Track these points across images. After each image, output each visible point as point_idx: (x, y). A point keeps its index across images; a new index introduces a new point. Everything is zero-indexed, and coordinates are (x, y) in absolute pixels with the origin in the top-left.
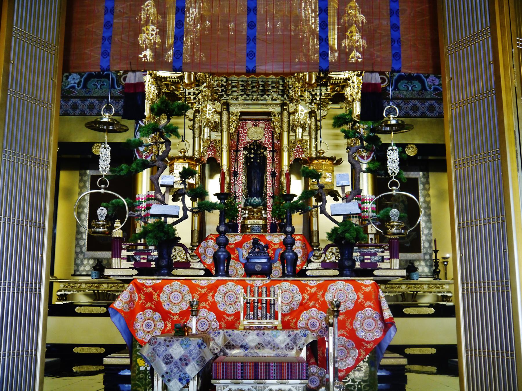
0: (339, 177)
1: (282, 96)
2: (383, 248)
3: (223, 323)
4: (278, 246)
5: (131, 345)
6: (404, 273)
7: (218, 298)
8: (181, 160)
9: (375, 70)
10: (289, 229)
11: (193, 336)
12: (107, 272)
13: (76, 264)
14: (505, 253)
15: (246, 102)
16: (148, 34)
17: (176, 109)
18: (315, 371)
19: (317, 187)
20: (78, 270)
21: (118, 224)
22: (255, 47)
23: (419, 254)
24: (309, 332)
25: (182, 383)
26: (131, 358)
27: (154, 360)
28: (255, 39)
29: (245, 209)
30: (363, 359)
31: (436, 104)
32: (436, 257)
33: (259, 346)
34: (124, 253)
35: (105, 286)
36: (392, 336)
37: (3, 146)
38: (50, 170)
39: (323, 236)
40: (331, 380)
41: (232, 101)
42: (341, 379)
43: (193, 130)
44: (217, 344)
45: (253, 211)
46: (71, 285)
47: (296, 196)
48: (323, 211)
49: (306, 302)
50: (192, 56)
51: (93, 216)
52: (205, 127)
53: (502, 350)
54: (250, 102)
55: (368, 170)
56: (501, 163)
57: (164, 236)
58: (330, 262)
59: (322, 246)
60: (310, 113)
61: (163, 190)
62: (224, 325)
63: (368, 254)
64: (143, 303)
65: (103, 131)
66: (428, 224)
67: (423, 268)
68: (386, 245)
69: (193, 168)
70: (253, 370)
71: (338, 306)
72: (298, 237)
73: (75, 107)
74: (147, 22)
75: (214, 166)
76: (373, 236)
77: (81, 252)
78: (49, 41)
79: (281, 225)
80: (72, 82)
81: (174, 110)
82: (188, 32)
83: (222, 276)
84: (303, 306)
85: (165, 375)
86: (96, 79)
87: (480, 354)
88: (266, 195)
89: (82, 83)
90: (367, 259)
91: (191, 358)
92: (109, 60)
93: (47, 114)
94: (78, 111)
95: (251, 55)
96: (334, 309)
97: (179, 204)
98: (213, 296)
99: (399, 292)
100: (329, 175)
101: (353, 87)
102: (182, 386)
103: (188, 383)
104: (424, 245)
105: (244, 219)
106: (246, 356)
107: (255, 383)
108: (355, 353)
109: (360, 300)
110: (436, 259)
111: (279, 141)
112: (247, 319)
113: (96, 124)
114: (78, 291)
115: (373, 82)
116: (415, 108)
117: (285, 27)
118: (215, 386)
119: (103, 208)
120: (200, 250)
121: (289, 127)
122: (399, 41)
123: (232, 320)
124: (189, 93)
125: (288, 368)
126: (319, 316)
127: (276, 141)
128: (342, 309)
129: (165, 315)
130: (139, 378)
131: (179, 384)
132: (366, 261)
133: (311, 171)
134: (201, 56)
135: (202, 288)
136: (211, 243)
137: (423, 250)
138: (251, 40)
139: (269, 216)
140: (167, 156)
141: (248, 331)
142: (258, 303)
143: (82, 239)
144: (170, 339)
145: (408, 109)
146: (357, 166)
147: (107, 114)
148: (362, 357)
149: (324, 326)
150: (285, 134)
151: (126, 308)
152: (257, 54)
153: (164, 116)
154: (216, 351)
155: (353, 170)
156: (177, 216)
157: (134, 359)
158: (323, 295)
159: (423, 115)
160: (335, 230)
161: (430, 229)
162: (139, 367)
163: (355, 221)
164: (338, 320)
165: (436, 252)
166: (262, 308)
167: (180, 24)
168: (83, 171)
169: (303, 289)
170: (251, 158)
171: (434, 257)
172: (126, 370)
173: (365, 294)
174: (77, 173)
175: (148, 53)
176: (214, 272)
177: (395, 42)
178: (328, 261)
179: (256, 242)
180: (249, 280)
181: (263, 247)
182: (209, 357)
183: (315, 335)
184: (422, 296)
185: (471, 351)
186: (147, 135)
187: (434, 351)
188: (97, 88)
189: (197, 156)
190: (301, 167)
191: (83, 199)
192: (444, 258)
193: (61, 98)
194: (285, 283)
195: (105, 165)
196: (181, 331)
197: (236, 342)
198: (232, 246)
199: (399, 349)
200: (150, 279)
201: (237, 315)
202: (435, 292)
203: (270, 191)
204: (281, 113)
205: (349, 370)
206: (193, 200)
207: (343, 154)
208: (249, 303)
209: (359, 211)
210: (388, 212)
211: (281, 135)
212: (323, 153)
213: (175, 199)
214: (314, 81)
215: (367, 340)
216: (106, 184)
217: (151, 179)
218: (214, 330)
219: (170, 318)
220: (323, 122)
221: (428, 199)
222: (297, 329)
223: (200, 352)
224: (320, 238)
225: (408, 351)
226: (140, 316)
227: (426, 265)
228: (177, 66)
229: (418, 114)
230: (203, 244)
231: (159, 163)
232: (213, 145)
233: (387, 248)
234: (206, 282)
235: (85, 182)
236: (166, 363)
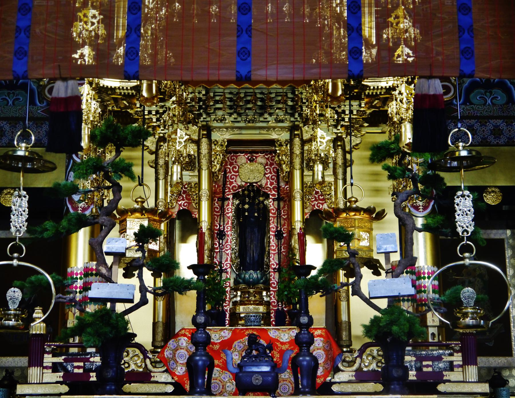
0: (381, 239)
1: (292, 115)
2: (452, 348)
4: (287, 346)
8: (138, 215)
9: (434, 75)
10: (304, 320)
15: (237, 125)
16: (86, 23)
17: (129, 137)
19: (346, 255)
21: (38, 314)
22: (250, 42)
23: (509, 358)
28: (249, 30)
29: (236, 290)
34: (48, 359)
39: (357, 330)
41: (215, 124)
47: (314, 268)
48: (357, 292)
50: (154, 56)
52: (174, 163)
54: (242, 124)
55: (426, 228)
59: (356, 345)
63: (427, 358)
65: (18, 170)
69: (155, 225)
72: (319, 332)
75: (189, 223)
79: (292, 313)
82: (147, 19)
86: (6, 92)
88: (268, 266)
90: (427, 366)
95: (244, 54)
97: (135, 281)
100: (364, 235)
101: (401, 101)
105: (235, 304)
111: (287, 183)
113: (6, 160)
115: (432, 93)
119: (16, 289)
120: (167, 353)
121: (302, 162)
122: (471, 29)
124: (150, 112)
127: (282, 184)
132: (425, 369)
133: (337, 230)
134: (167, 55)
136: (184, 341)
138: (244, 30)
139: (273, 300)
140: (116, 207)
146: (408, 222)
147: (24, 145)
150: (297, 174)
153: (111, 147)
156: (131, 301)
160: (375, 321)
163: (406, 306)
170: (245, 210)
176: (187, 387)
177: (465, 31)
178: (365, 369)
179: (253, 341)
181: (264, 348)
186: (85, 176)
198: (217, 347)
203: (274, 261)
204: (290, 142)
206: (156, 275)
207: (386, 202)
209: (412, 291)
211: (290, 174)
212: (356, 201)
213: (127, 275)
214: (340, 93)
217: (91, 244)
220: (355, 153)
228: (131, 70)
230: (172, 343)
233: (457, 348)
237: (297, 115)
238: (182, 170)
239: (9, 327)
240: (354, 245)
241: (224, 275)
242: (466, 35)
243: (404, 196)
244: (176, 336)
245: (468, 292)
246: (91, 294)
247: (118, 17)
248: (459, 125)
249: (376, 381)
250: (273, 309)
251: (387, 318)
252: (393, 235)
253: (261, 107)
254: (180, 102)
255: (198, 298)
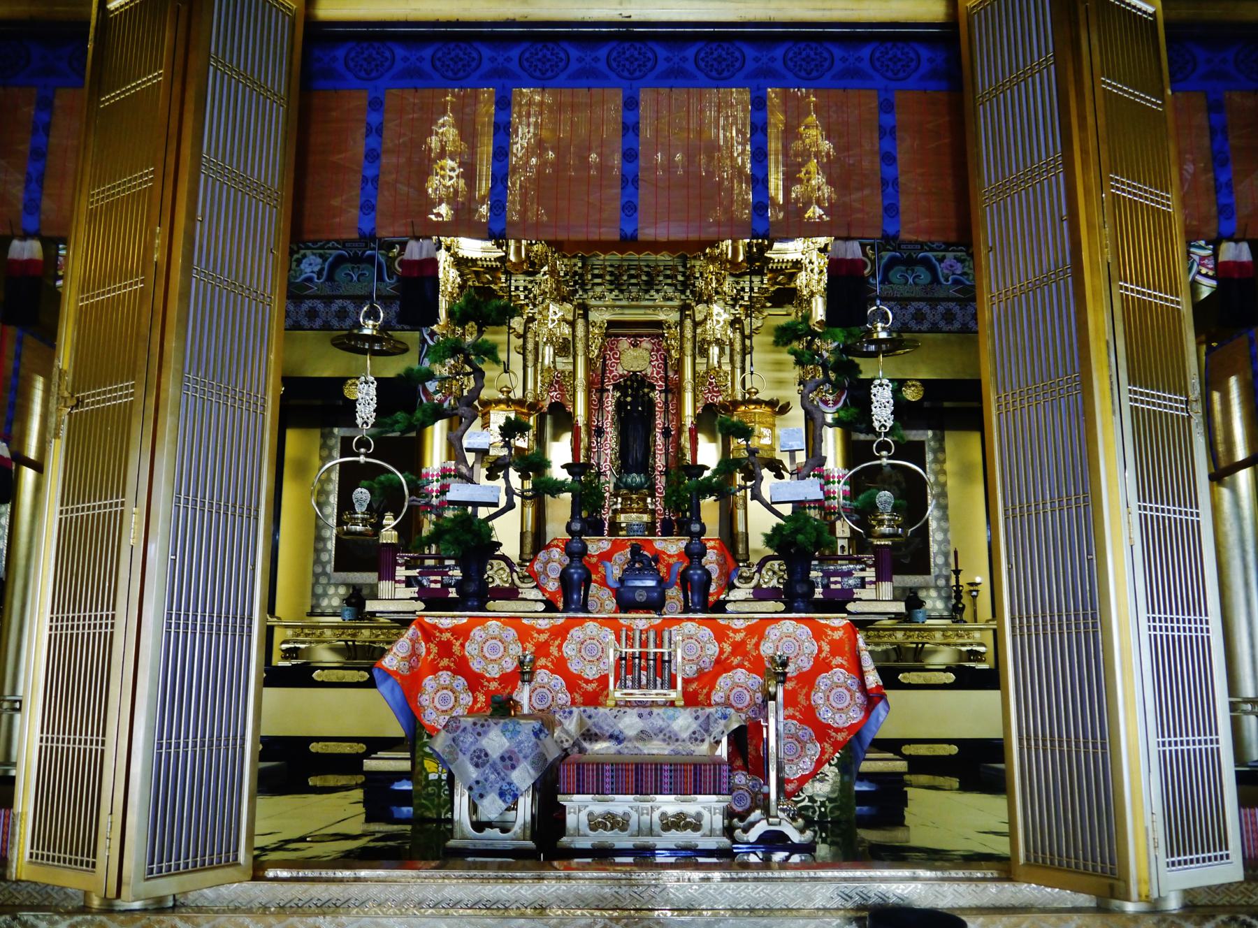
0: (783, 436)
1: (683, 292)
2: (864, 563)
3: (577, 696)
4: (675, 559)
5: (414, 737)
6: (900, 607)
7: (569, 649)
8: (503, 406)
9: (853, 235)
10: (695, 528)
11: (525, 717)
12: (371, 606)
13: (315, 595)
14: (1090, 561)
15: (618, 303)
16: (443, 177)
17: (494, 314)
18: (743, 782)
19: (745, 454)
20: (318, 606)
21: (389, 521)
22: (636, 195)
23: (927, 577)
24: (732, 711)
25: (504, 801)
26: (413, 759)
27: (455, 760)
28: (635, 181)
29: (616, 496)
30: (828, 761)
31: (956, 309)
32: (957, 581)
33: (643, 736)
34: (401, 573)
35: (366, 633)
36: (881, 719)
37: (183, 369)
38: (268, 415)
39: (757, 543)
40: (773, 796)
41: (593, 302)
42: (789, 795)
43: (524, 355)
44: (567, 732)
45: (631, 499)
46: (306, 631)
47: (708, 468)
48: (756, 496)
49: (727, 658)
50: (523, 214)
51: (346, 504)
52: (545, 344)
53: (1085, 737)
54: (624, 303)
55: (838, 423)
56: (1083, 399)
57: (472, 541)
58: (768, 589)
59: (754, 559)
60: (732, 323)
61: (471, 458)
62: (579, 699)
63: (836, 573)
64: (434, 660)
65: (364, 352)
66: (943, 524)
67: (934, 602)
68: (869, 558)
69: (524, 418)
70: (632, 779)
71: (784, 664)
72: (711, 544)
73: (313, 314)
74: (442, 155)
75: (561, 418)
76: (845, 543)
77: (324, 573)
78: (266, 182)
79: (681, 519)
80: (308, 270)
81: (490, 315)
82: (515, 170)
83: (576, 611)
84: (722, 665)
85: (475, 787)
86: (349, 265)
87: (1044, 744)
88: (654, 469)
89: (325, 273)
90: (836, 583)
91: (521, 756)
92: (375, 218)
93: (263, 314)
94: (318, 323)
95: (630, 208)
96: (777, 670)
97: (500, 483)
98: (560, 647)
99: (892, 644)
100: (766, 432)
101: (812, 271)
102: (504, 806)
103: (516, 797)
104: (936, 560)
105: (615, 512)
106: (620, 753)
107: (636, 800)
108: (814, 750)
109: (824, 655)
110: (958, 585)
111: (676, 372)
112: (620, 687)
113: (350, 340)
114: (318, 642)
115: (849, 257)
116: (919, 317)
117: (690, 157)
118: (564, 807)
119: (364, 490)
120: (537, 567)
121: (694, 347)
122: (895, 181)
123: (594, 690)
124: (517, 288)
125: (695, 774)
126: (750, 682)
127: (671, 374)
128: (791, 670)
129: (475, 682)
130: (429, 794)
131: (500, 802)
132: (833, 586)
133: (734, 424)
134: (539, 213)
135: (540, 632)
136: (556, 553)
137: (934, 570)
138: (630, 181)
139: (659, 507)
140: (478, 397)
141: (622, 710)
142: (640, 658)
143: (325, 549)
144: (482, 721)
145: (907, 317)
146: (817, 415)
147: (371, 322)
148: (827, 756)
149: (759, 701)
150: (688, 361)
151: (404, 668)
152: (640, 208)
153: (471, 326)
154: (566, 745)
155: (811, 423)
156: (496, 505)
157: (419, 760)
158: (757, 645)
159: (934, 329)
160: (777, 529)
161: (945, 531)
162: (427, 774)
163: (813, 513)
164: (784, 690)
165: (957, 572)
166: (647, 669)
167: (502, 153)
168: (327, 430)
169: (720, 634)
170: (627, 403)
171: (953, 582)
172: (404, 781)
173: (832, 643)
174: (316, 434)
175: (444, 209)
176: (561, 605)
177: (889, 184)
178: (764, 586)
179: (636, 550)
180: (625, 618)
181: (649, 560)
182: (553, 754)
183: (743, 716)
184: (933, 652)
185: (1028, 740)
186: (440, 360)
187: (954, 750)
188: (351, 280)
189: (530, 399)
190: (720, 419)
191: (329, 470)
192: (972, 584)
193: (288, 298)
194: (689, 624)
195: (366, 411)
196: (503, 708)
197: (601, 728)
198: (594, 560)
199: (893, 746)
200: (447, 617)
201: (603, 680)
202: (955, 645)
203: (660, 462)
204: (681, 323)
205: (803, 780)
206: (524, 477)
207: (792, 394)
208: (625, 659)
209: (820, 496)
210: (873, 498)
211: (680, 362)
212: (756, 393)
213: (491, 477)
214: (741, 258)
215: (835, 725)
216: (368, 446)
217: (448, 439)
218: (562, 707)
219: (483, 686)
220: (755, 338)
221: (942, 478)
222: (710, 705)
223: (537, 745)
224: (751, 545)
225: (908, 750)
226: (429, 682)
227: (940, 597)
228: (497, 228)
229: (925, 327)
230: (542, 555)
231: (463, 410)
232: (561, 382)
233: (870, 562)
234: (547, 621)
235: (331, 449)
236: (477, 765)
237: (688, 292)
238: (555, 354)
239: (355, 533)
240: (754, 442)
241: (603, 479)
242: (890, 190)
243: (813, 385)
244: (548, 547)
245: (885, 497)
246: (450, 496)
247: (481, 164)
248: (878, 302)
249: (777, 599)
250: (659, 518)
251: (791, 525)
252: (800, 430)
253: (646, 283)
254: (553, 272)
255: (573, 502)
